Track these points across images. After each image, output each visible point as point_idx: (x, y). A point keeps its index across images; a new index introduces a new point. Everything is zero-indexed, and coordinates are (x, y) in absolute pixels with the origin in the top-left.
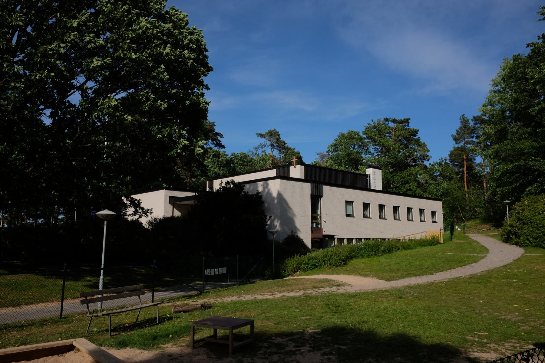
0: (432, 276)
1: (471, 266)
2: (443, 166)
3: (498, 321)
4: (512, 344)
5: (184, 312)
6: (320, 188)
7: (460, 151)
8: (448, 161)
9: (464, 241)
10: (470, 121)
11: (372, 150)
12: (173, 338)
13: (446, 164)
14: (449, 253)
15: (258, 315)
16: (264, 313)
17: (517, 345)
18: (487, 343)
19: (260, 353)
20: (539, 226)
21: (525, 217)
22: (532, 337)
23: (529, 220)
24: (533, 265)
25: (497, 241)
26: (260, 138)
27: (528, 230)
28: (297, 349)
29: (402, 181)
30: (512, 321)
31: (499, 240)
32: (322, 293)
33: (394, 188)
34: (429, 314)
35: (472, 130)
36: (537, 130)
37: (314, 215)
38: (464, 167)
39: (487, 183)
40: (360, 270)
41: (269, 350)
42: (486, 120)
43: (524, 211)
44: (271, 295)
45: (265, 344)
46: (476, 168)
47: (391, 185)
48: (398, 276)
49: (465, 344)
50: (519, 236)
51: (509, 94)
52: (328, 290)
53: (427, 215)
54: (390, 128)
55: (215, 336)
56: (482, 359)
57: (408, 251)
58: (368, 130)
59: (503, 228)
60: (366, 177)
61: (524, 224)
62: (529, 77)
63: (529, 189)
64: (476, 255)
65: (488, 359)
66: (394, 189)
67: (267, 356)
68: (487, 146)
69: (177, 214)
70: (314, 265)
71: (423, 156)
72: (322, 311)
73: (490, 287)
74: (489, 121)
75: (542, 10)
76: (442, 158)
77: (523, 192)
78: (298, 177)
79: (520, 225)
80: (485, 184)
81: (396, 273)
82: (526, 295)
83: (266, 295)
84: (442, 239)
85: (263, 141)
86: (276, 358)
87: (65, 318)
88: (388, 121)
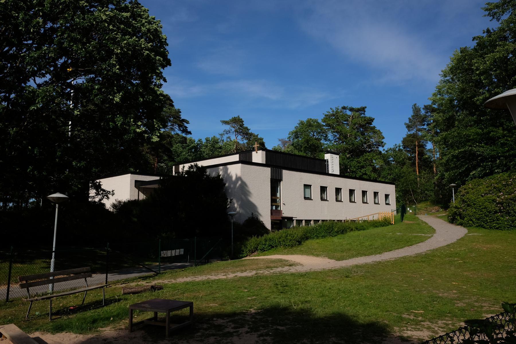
0: (380, 255)
1: (418, 246)
2: (396, 152)
3: (435, 299)
4: (445, 322)
5: (134, 293)
6: (280, 172)
7: (412, 137)
8: (401, 148)
9: (414, 222)
10: (421, 109)
11: (330, 136)
12: (113, 321)
13: (399, 150)
14: (398, 234)
15: (206, 296)
16: (213, 293)
17: (450, 322)
18: (421, 321)
19: (197, 336)
20: (482, 207)
21: (469, 200)
22: (465, 315)
23: (473, 202)
24: (474, 244)
25: (444, 221)
26: (224, 125)
27: (472, 212)
28: (235, 330)
29: (358, 166)
30: (448, 298)
31: (445, 221)
32: (273, 273)
33: (351, 172)
34: (371, 293)
35: (423, 118)
36: (482, 118)
37: (274, 198)
38: (416, 153)
39: (437, 167)
40: (314, 250)
41: (207, 332)
42: (436, 109)
43: (468, 193)
44: (224, 275)
45: (205, 325)
46: (427, 154)
47: (349, 170)
48: (348, 256)
49: (401, 323)
50: (463, 217)
51: (458, 85)
52: (280, 270)
53: (381, 198)
54: (347, 115)
55: (155, 318)
56: (414, 337)
57: (361, 232)
58: (327, 118)
59: (449, 209)
60: (325, 162)
61: (468, 205)
62: (475, 68)
63: (473, 173)
64: (423, 235)
65: (420, 338)
66: (351, 173)
67: (203, 338)
68: (437, 133)
69: (142, 197)
70: (271, 245)
71: (378, 143)
72: (269, 291)
73: (433, 265)
74: (438, 109)
75: (487, 6)
76: (396, 145)
77: (467, 175)
78: (260, 161)
79: (464, 207)
80: (434, 169)
81: (347, 253)
82: (465, 273)
83: (219, 276)
84: (393, 220)
85: (227, 127)
86: (212, 339)
87: (12, 301)
88: (346, 109)
